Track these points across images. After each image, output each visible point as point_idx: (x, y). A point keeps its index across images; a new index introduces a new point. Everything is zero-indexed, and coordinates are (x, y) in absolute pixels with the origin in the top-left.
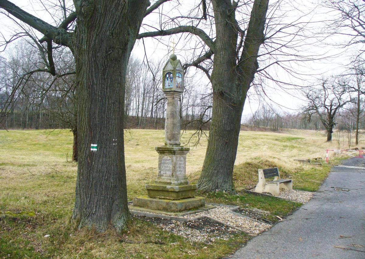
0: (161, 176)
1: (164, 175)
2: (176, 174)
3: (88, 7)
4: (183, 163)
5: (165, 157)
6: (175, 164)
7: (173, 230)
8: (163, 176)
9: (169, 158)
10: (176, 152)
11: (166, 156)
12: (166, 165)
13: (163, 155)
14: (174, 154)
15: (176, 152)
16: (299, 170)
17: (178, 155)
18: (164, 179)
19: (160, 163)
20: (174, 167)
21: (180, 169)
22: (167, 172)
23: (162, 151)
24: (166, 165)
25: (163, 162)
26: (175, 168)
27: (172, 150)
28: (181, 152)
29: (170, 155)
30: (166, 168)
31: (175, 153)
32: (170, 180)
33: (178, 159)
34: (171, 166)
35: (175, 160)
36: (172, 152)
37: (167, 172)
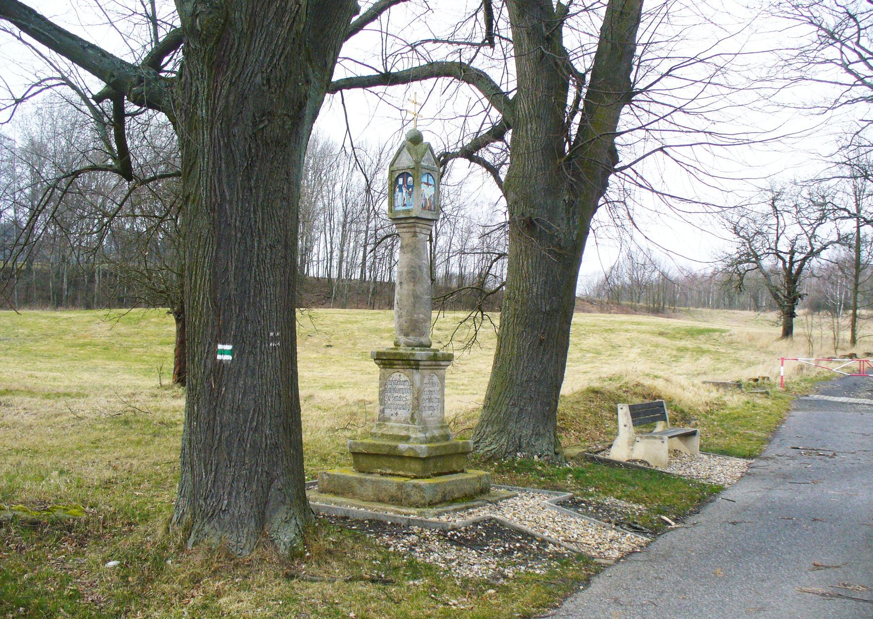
1: (393, 418)
5: (396, 376)
6: (420, 392)
8: (389, 419)
9: (404, 378)
11: (398, 374)
12: (396, 395)
13: (389, 370)
14: (417, 369)
15: (421, 363)
17: (426, 372)
18: (392, 427)
20: (417, 399)
24: (396, 395)
25: (389, 386)
27: (411, 358)
28: (434, 363)
29: (407, 371)
30: (397, 402)
33: (426, 381)
34: (409, 397)
35: (418, 383)
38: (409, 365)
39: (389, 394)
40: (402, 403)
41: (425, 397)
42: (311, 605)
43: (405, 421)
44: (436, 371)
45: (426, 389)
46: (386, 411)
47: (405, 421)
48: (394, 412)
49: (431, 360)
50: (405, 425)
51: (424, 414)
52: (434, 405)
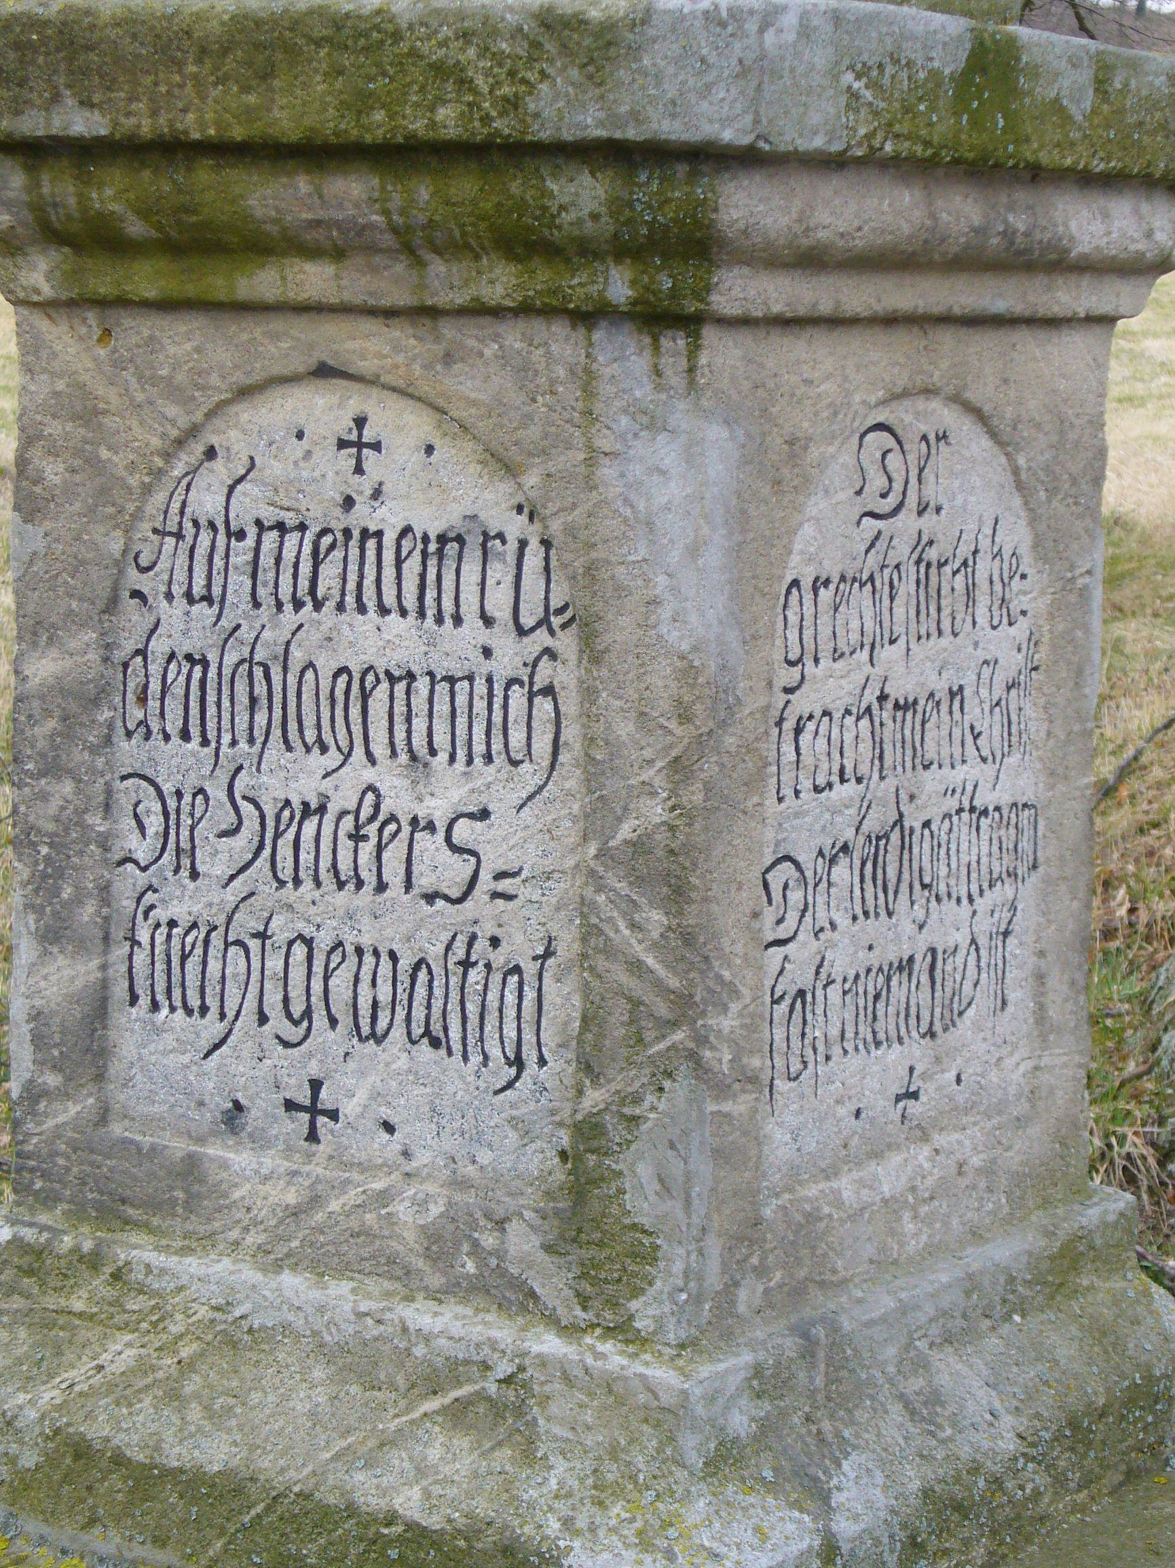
0: (112, 1210)
1: (256, 1173)
2: (737, 1151)
3: (408, 79)
4: (1005, 646)
5: (285, 447)
6: (713, 742)
7: (1149, 925)
8: (178, 1195)
9: (423, 484)
10: (745, 205)
11: (327, 410)
12: (291, 776)
13: (180, 342)
14: (665, 319)
15: (745, 205)
16: (387, 1233)
17: (836, 378)
18: (235, 1338)
19: (78, 702)
20: (668, 873)
21: (900, 935)
22: (362, 1081)
23: (111, 194)
24: (291, 776)
25: (182, 628)
26: (689, 943)
27: (564, 107)
28: (961, 212)
29: (491, 369)
30: (327, 913)
31: (698, 245)
32: (501, 1409)
33: (824, 533)
34: (525, 827)
35: (684, 602)
36: (582, 196)
37: (362, 1081)
38: (526, 242)
39: (178, 763)
40: (403, 926)
41: (809, 822)
42: (558, 909)
43: (455, 1257)
44: (981, 361)
45: (832, 685)
46: (129, 1028)
47: (455, 1257)
48: (257, 1069)
49: (924, 167)
50: (446, 1324)
51: (790, 1129)
52: (951, 926)
